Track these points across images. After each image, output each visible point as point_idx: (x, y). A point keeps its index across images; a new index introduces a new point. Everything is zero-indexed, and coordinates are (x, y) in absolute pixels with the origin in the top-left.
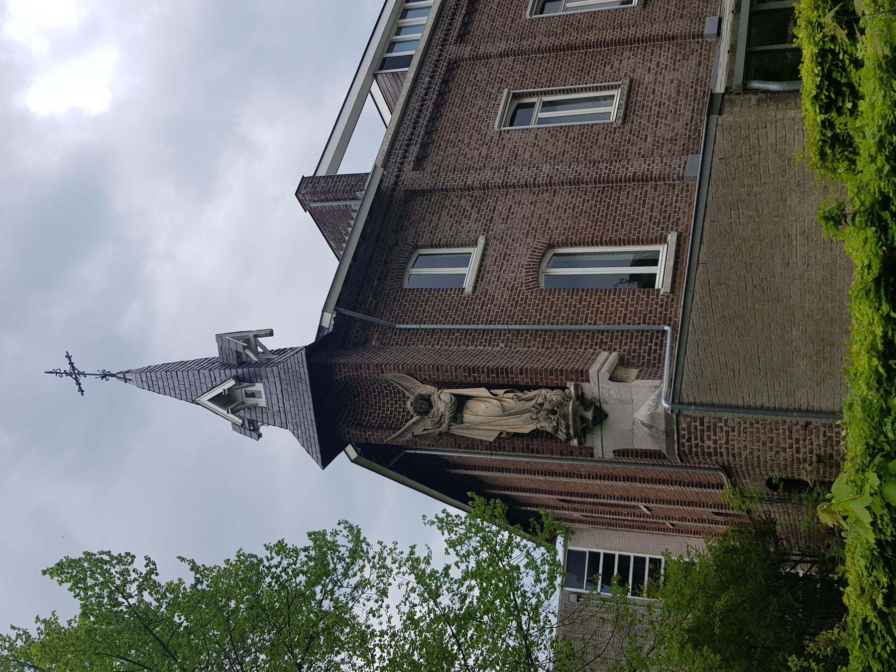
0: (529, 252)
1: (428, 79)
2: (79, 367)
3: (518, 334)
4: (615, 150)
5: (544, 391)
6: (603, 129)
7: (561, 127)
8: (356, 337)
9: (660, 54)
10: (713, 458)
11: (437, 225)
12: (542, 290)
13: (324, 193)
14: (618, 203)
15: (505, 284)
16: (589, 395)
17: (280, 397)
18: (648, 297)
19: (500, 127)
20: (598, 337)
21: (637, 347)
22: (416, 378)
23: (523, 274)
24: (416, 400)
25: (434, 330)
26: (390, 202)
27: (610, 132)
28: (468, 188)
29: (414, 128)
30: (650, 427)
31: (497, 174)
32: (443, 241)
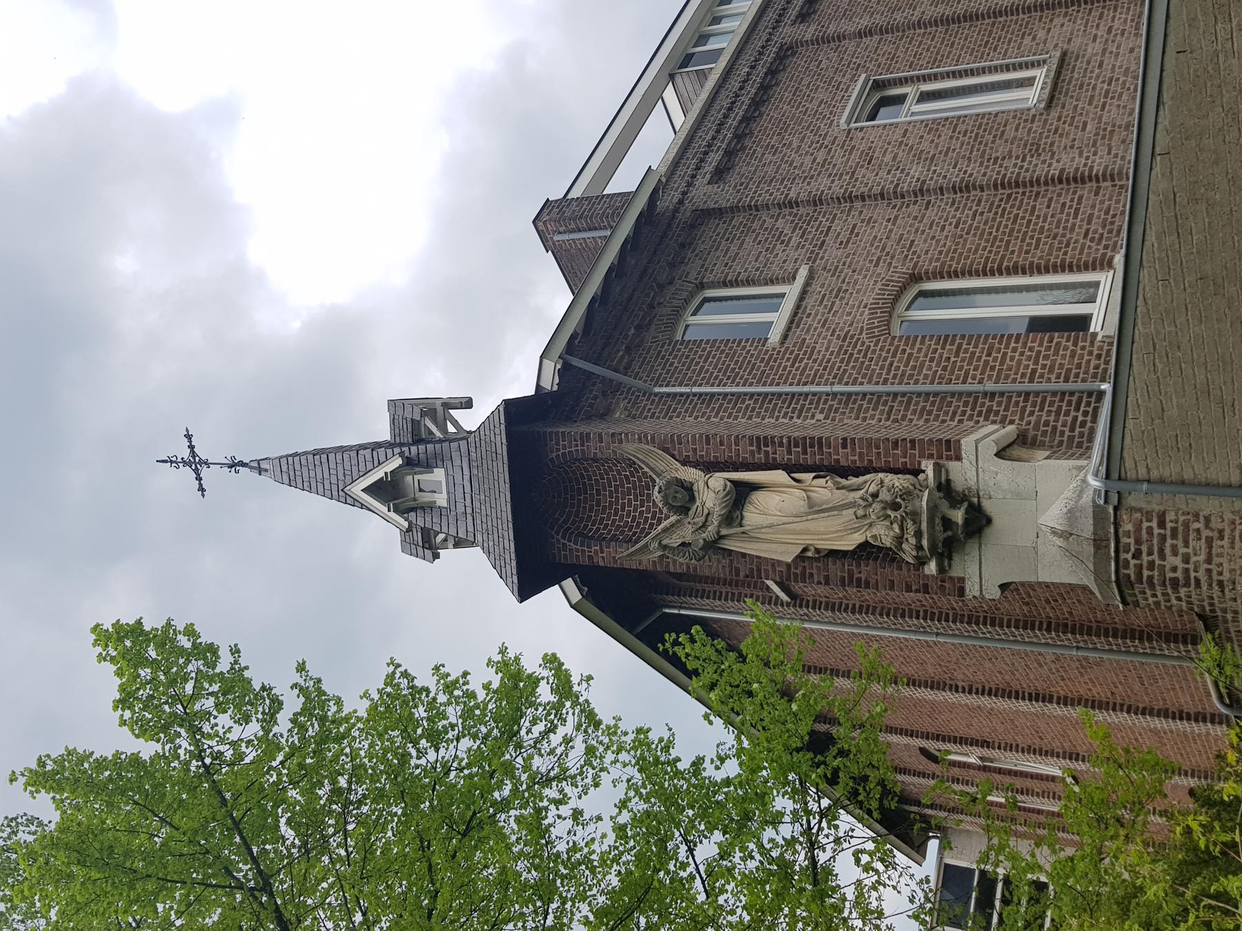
0: (879, 285)
1: (746, 70)
2: (202, 453)
3: (848, 400)
4: (1032, 144)
5: (881, 475)
6: (1014, 117)
7: (947, 119)
8: (591, 405)
9: (1114, 17)
10: (1183, 591)
11: (737, 254)
12: (894, 338)
13: (574, 220)
14: (1032, 214)
15: (834, 331)
16: (959, 484)
17: (468, 489)
18: (1075, 344)
19: (848, 122)
20: (983, 405)
21: (1052, 418)
22: (673, 456)
23: (866, 316)
24: (669, 484)
25: (713, 395)
26: (669, 225)
27: (1026, 121)
28: (790, 202)
29: (718, 131)
30: (1066, 535)
31: (836, 182)
32: (743, 276)
